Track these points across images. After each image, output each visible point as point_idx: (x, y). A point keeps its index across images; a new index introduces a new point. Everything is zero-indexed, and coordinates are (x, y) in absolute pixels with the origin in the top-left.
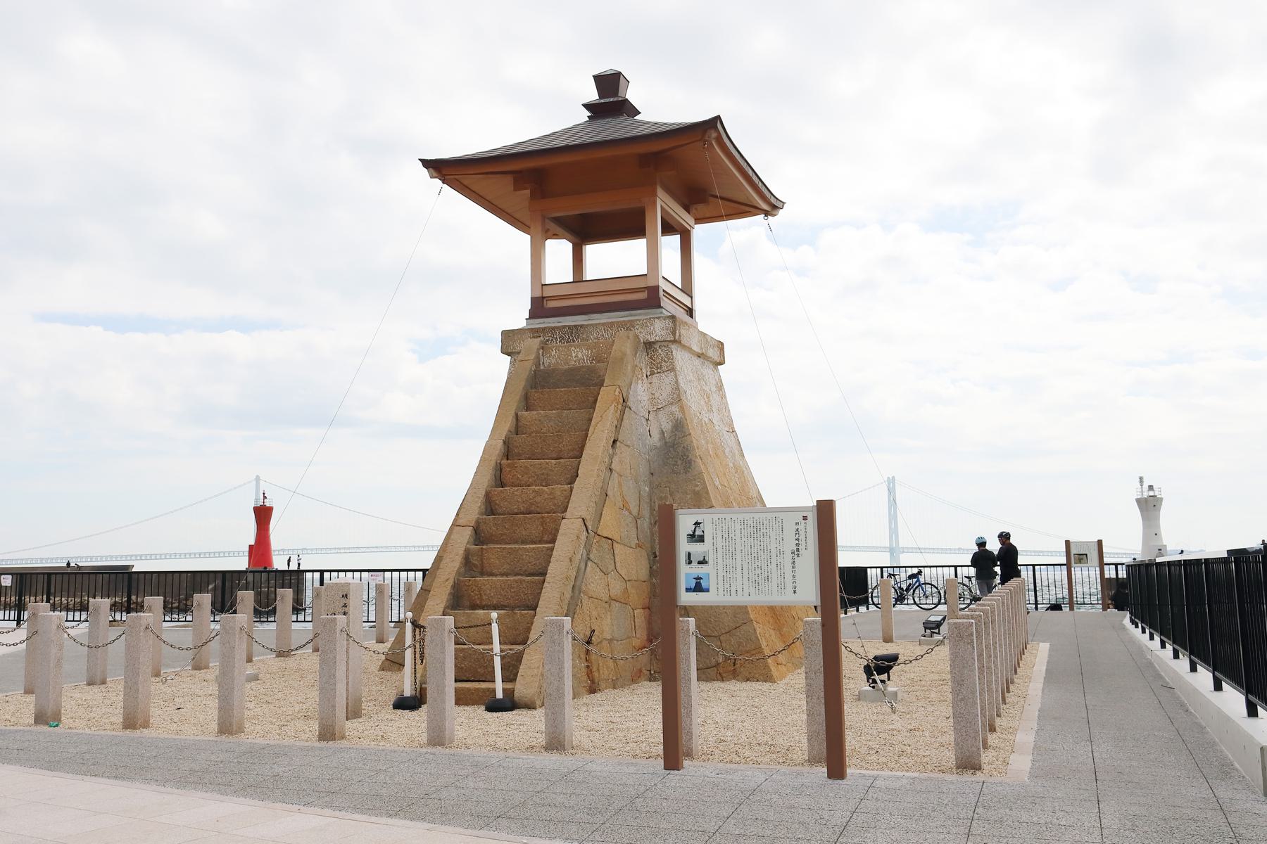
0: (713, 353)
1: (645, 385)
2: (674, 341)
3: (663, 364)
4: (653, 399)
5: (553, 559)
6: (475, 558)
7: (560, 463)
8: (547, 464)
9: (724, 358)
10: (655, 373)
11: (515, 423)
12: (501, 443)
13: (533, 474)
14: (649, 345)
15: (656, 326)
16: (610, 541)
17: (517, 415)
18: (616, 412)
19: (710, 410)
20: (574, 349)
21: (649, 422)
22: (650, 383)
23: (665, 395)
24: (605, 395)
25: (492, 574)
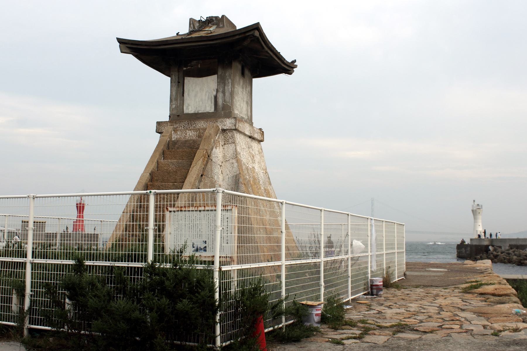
0: (257, 136)
1: (221, 150)
2: (236, 130)
3: (230, 140)
4: (224, 156)
8: (168, 185)
9: (263, 138)
11: (157, 165)
12: (148, 174)
14: (224, 131)
15: (227, 122)
17: (158, 162)
18: (203, 161)
19: (254, 162)
22: (224, 149)
23: (230, 155)
24: (199, 154)
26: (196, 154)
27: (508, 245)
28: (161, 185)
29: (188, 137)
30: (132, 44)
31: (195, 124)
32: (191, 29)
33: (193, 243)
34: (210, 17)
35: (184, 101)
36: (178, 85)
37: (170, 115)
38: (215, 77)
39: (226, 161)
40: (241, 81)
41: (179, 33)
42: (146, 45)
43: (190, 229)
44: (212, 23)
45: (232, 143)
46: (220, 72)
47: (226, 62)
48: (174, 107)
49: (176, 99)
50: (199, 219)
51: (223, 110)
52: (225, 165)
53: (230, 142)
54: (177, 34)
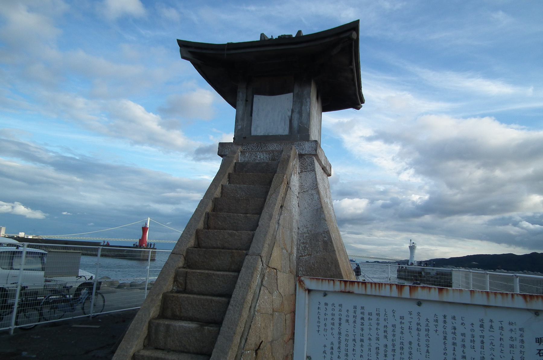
3: (309, 167)
5: (237, 286)
6: (181, 278)
10: (303, 172)
13: (228, 222)
15: (306, 145)
16: (275, 270)
20: (259, 153)
21: (298, 198)
25: (191, 292)
27: (430, 272)
28: (228, 217)
30: (196, 48)
31: (266, 146)
36: (246, 104)
38: (290, 96)
40: (316, 104)
42: (212, 49)
45: (311, 170)
48: (240, 128)
50: (414, 326)
52: (302, 196)
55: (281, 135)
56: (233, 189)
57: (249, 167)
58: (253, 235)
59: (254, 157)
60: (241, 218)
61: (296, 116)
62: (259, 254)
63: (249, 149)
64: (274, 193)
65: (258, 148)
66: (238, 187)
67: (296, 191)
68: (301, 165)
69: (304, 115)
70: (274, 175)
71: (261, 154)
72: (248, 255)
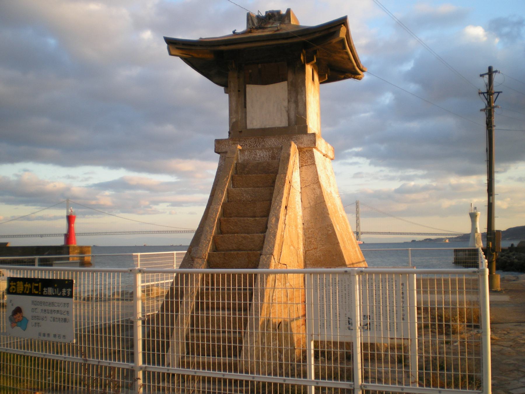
7: (256, 220)
8: (248, 220)
10: (303, 166)
13: (240, 226)
16: (285, 266)
26: (276, 180)
28: (238, 221)
29: (259, 158)
31: (264, 141)
32: (249, 26)
33: (349, 318)
34: (270, 12)
35: (247, 114)
37: (230, 130)
39: (306, 186)
41: (235, 30)
43: (344, 298)
44: (273, 18)
46: (290, 77)
47: (298, 66)
49: (237, 112)
51: (296, 124)
53: (309, 163)
54: (234, 32)
55: (278, 128)
56: (239, 193)
57: (250, 168)
58: (264, 237)
59: (254, 155)
60: (251, 222)
61: (293, 106)
62: (271, 253)
63: (247, 144)
64: (278, 195)
65: (256, 143)
66: (243, 190)
67: (298, 187)
68: (301, 158)
69: (300, 105)
70: (276, 176)
71: (261, 152)
72: (262, 255)
